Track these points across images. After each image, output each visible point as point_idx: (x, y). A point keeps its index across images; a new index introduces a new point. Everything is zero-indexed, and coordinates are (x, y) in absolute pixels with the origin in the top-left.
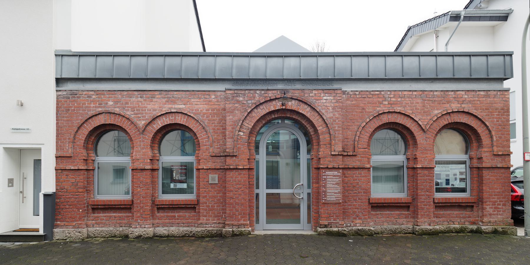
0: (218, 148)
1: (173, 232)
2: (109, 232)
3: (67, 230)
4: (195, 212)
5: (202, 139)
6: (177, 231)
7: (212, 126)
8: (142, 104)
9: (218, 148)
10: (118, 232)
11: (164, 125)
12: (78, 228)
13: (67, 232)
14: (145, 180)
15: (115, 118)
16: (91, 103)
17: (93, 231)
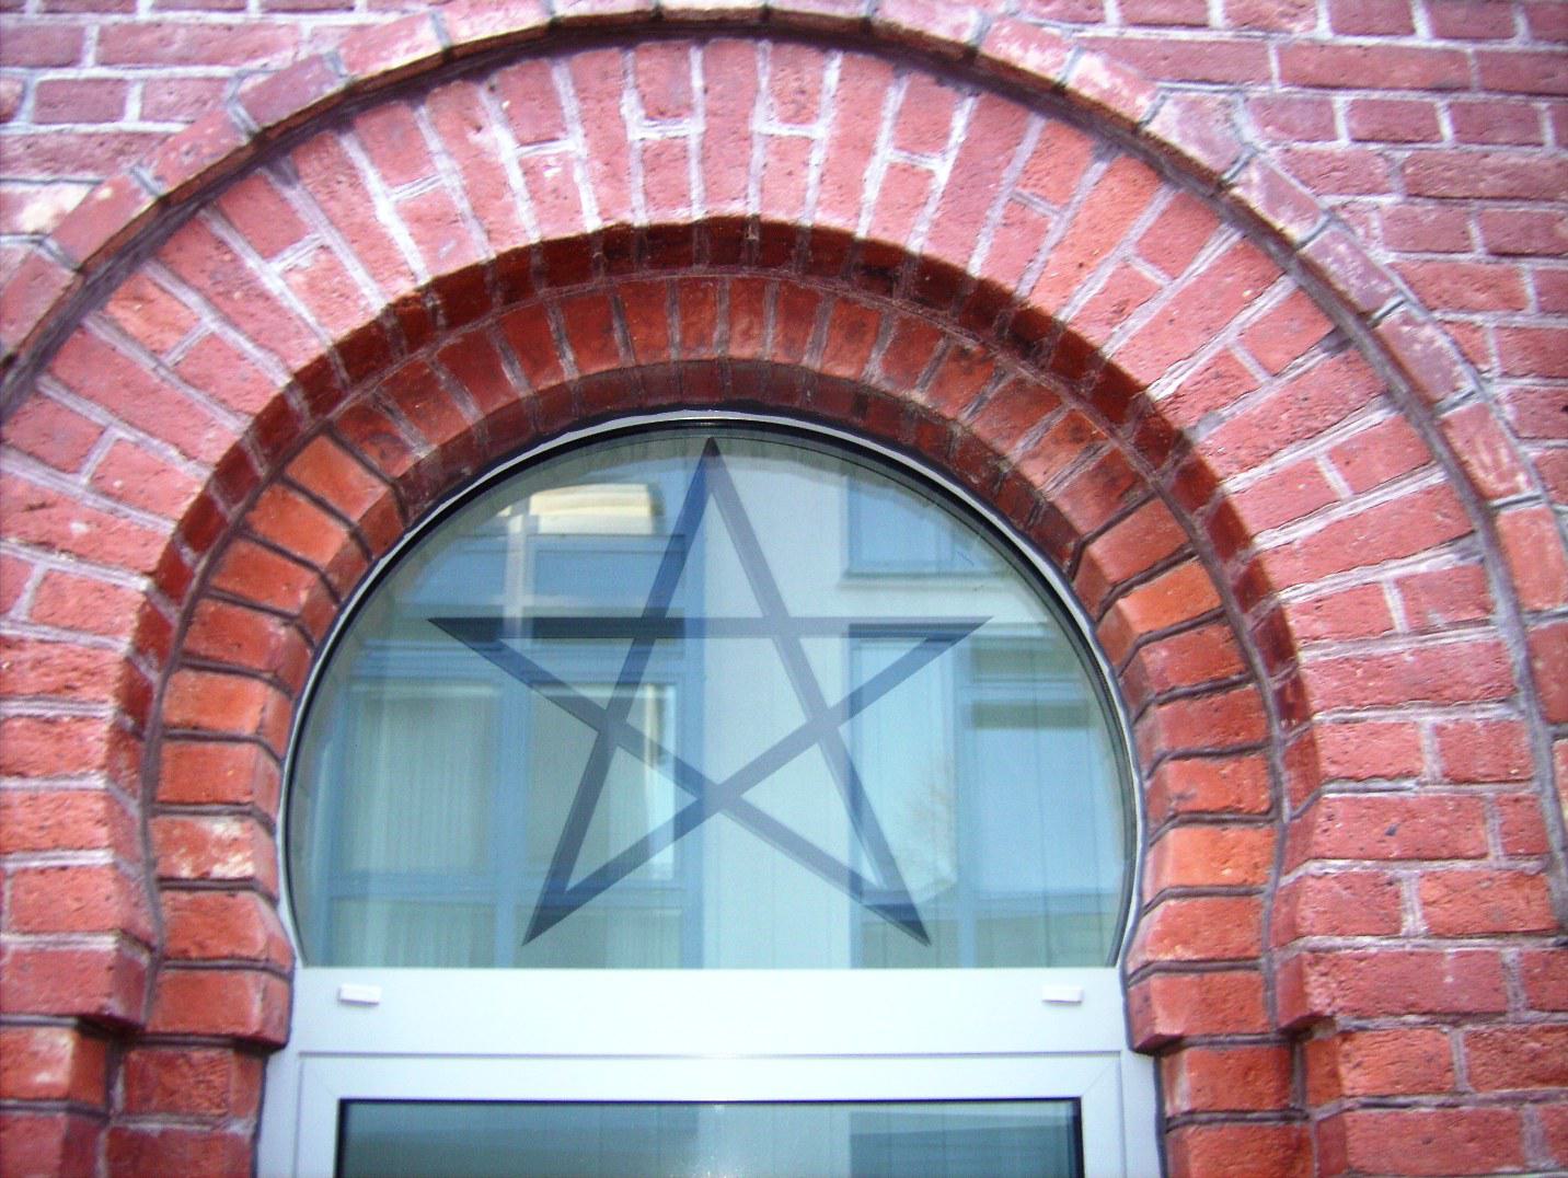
5: (1328, 553)
7: (1513, 303)
11: (480, 251)
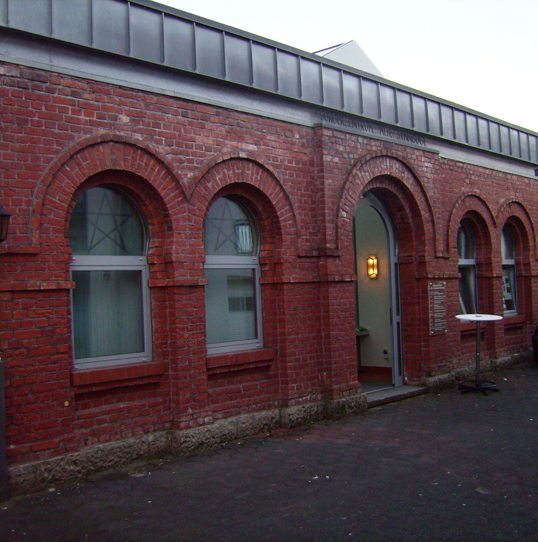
0: (307, 241)
1: (244, 426)
2: (126, 450)
3: (43, 464)
4: (269, 377)
6: (251, 421)
7: (297, 195)
8: (186, 131)
9: (307, 241)
10: (145, 447)
12: (67, 451)
13: (43, 468)
14: (196, 311)
15: (134, 159)
16: (78, 113)
17: (92, 456)
